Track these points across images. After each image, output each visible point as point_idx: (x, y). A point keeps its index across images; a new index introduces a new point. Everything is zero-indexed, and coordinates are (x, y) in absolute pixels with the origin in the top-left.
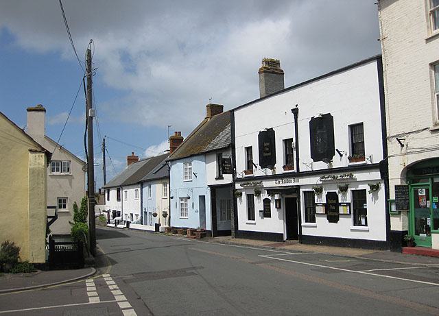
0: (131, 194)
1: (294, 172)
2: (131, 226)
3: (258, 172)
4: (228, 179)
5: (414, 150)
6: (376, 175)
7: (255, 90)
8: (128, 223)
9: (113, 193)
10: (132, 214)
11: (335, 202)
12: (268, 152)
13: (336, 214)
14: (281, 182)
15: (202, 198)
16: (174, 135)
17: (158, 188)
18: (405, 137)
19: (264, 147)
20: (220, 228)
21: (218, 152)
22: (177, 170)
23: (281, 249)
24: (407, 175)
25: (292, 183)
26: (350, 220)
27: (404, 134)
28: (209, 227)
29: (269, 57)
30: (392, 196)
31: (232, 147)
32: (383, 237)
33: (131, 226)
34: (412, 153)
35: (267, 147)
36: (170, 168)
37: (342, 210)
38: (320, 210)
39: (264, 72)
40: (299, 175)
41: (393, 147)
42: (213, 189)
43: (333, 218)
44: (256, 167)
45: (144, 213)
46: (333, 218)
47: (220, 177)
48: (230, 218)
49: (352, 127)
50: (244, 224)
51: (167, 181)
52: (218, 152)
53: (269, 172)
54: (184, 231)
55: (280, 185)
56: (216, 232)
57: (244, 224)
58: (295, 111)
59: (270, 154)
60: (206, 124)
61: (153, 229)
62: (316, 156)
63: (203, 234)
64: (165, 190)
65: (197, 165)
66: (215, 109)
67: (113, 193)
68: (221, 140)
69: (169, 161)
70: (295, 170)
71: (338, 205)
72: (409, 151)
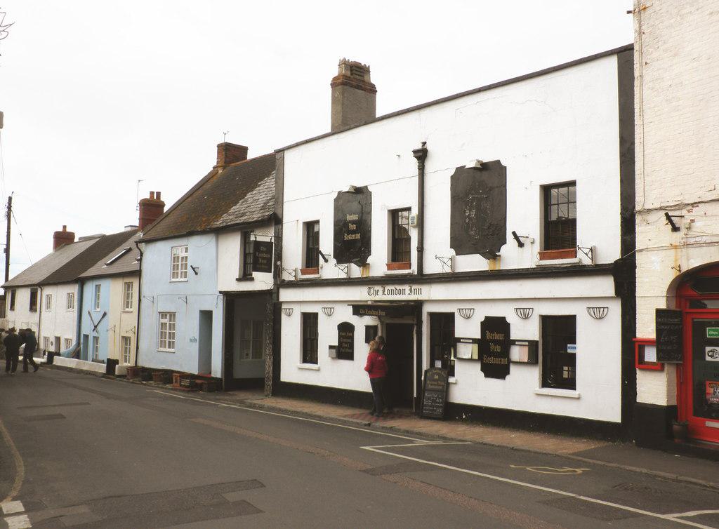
0: (59, 296)
1: (411, 275)
2: (58, 361)
3: (330, 269)
4: (262, 281)
5: (705, 239)
6: (606, 286)
7: (323, 120)
8: (51, 356)
9: (23, 297)
10: (58, 339)
11: (500, 337)
12: (354, 232)
13: (504, 361)
14: (380, 293)
15: (207, 316)
16: (148, 196)
17: (113, 291)
18: (684, 212)
19: (346, 224)
20: (241, 372)
21: (245, 229)
22: (157, 257)
23: (384, 429)
24: (131, 370)
25: (406, 294)
26: (534, 374)
27: (679, 206)
28: (217, 369)
29: (353, 58)
30: (646, 328)
31: (275, 220)
32: (611, 412)
33: (58, 361)
34: (699, 245)
35: (353, 222)
36: (142, 255)
37: (517, 353)
38: (467, 351)
39: (343, 84)
40: (422, 278)
41: (649, 233)
42: (231, 299)
43: (495, 366)
44: (326, 261)
45: (82, 339)
46: (495, 366)
47: (245, 276)
48: (258, 353)
49: (546, 190)
50: (292, 370)
51: (136, 282)
52: (245, 229)
53: (356, 271)
54: (166, 377)
55: (377, 298)
56: (231, 383)
57: (292, 370)
58: (422, 155)
59: (358, 236)
60: (215, 179)
61: (102, 369)
62: (460, 244)
63: (199, 384)
64: (128, 296)
65: (198, 249)
66: (231, 153)
67: (23, 297)
68: (252, 205)
69: (141, 241)
70: (414, 269)
71: (508, 343)
72: (692, 241)
